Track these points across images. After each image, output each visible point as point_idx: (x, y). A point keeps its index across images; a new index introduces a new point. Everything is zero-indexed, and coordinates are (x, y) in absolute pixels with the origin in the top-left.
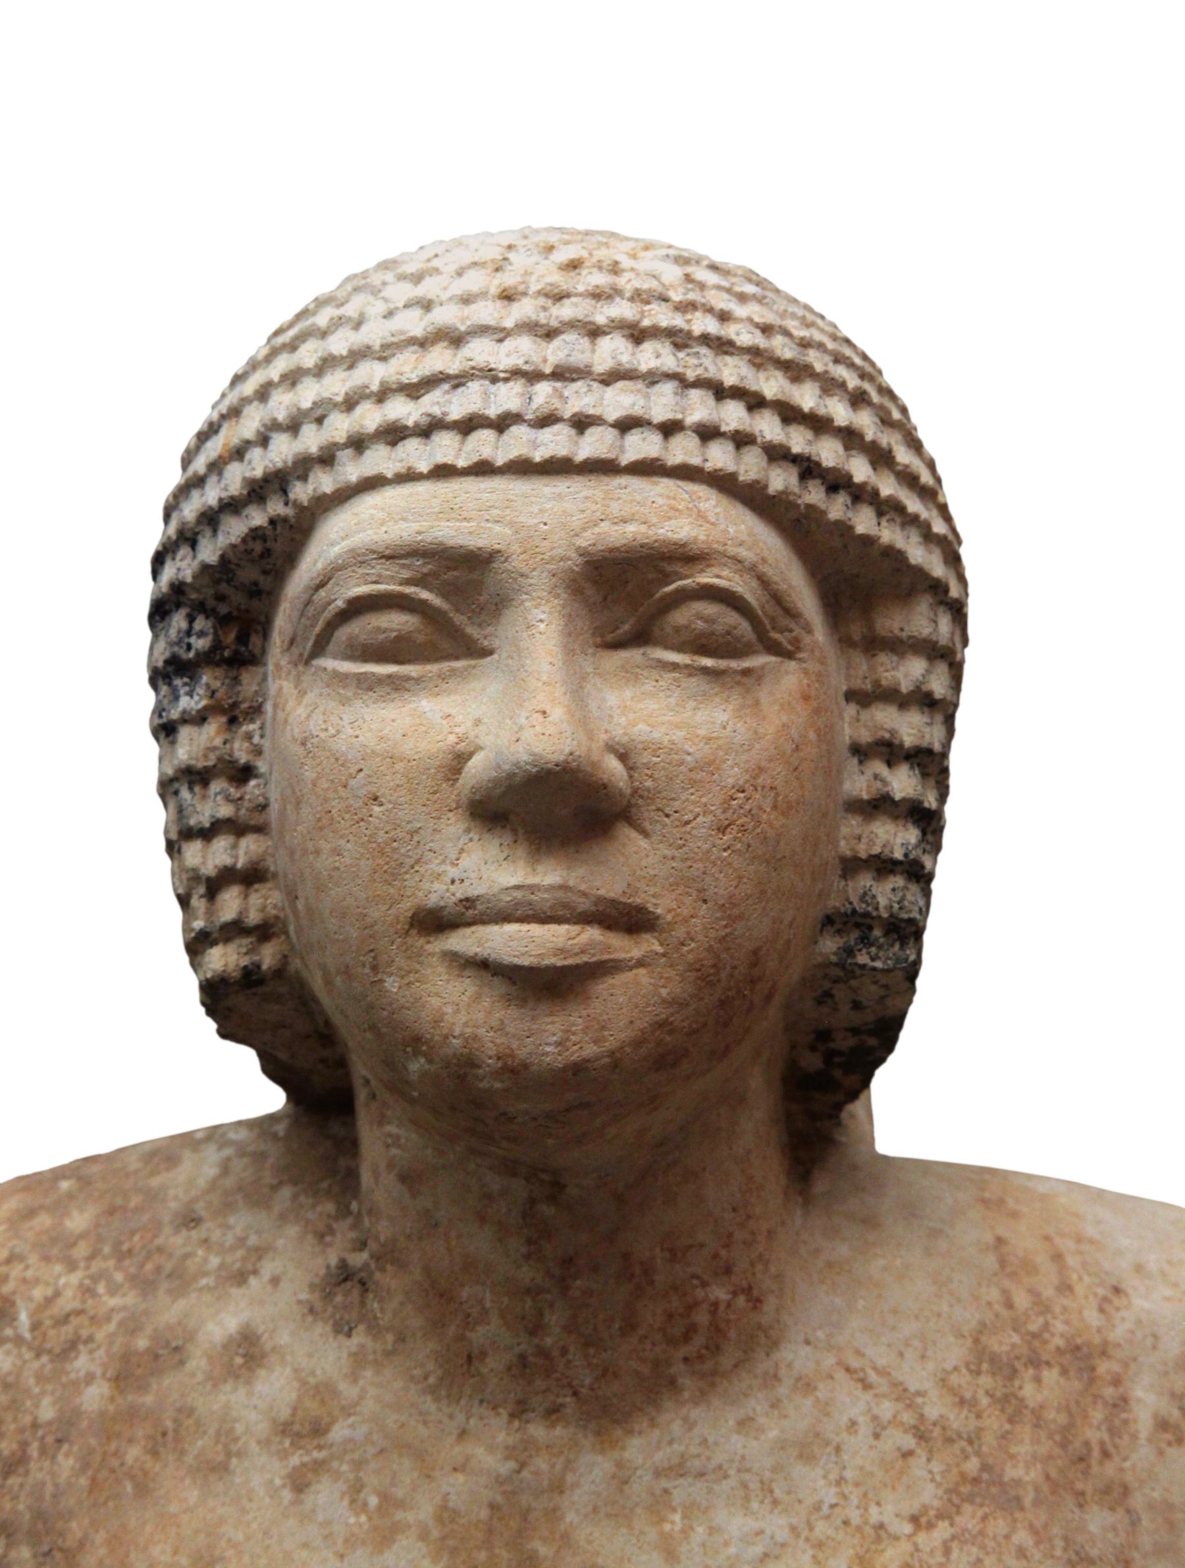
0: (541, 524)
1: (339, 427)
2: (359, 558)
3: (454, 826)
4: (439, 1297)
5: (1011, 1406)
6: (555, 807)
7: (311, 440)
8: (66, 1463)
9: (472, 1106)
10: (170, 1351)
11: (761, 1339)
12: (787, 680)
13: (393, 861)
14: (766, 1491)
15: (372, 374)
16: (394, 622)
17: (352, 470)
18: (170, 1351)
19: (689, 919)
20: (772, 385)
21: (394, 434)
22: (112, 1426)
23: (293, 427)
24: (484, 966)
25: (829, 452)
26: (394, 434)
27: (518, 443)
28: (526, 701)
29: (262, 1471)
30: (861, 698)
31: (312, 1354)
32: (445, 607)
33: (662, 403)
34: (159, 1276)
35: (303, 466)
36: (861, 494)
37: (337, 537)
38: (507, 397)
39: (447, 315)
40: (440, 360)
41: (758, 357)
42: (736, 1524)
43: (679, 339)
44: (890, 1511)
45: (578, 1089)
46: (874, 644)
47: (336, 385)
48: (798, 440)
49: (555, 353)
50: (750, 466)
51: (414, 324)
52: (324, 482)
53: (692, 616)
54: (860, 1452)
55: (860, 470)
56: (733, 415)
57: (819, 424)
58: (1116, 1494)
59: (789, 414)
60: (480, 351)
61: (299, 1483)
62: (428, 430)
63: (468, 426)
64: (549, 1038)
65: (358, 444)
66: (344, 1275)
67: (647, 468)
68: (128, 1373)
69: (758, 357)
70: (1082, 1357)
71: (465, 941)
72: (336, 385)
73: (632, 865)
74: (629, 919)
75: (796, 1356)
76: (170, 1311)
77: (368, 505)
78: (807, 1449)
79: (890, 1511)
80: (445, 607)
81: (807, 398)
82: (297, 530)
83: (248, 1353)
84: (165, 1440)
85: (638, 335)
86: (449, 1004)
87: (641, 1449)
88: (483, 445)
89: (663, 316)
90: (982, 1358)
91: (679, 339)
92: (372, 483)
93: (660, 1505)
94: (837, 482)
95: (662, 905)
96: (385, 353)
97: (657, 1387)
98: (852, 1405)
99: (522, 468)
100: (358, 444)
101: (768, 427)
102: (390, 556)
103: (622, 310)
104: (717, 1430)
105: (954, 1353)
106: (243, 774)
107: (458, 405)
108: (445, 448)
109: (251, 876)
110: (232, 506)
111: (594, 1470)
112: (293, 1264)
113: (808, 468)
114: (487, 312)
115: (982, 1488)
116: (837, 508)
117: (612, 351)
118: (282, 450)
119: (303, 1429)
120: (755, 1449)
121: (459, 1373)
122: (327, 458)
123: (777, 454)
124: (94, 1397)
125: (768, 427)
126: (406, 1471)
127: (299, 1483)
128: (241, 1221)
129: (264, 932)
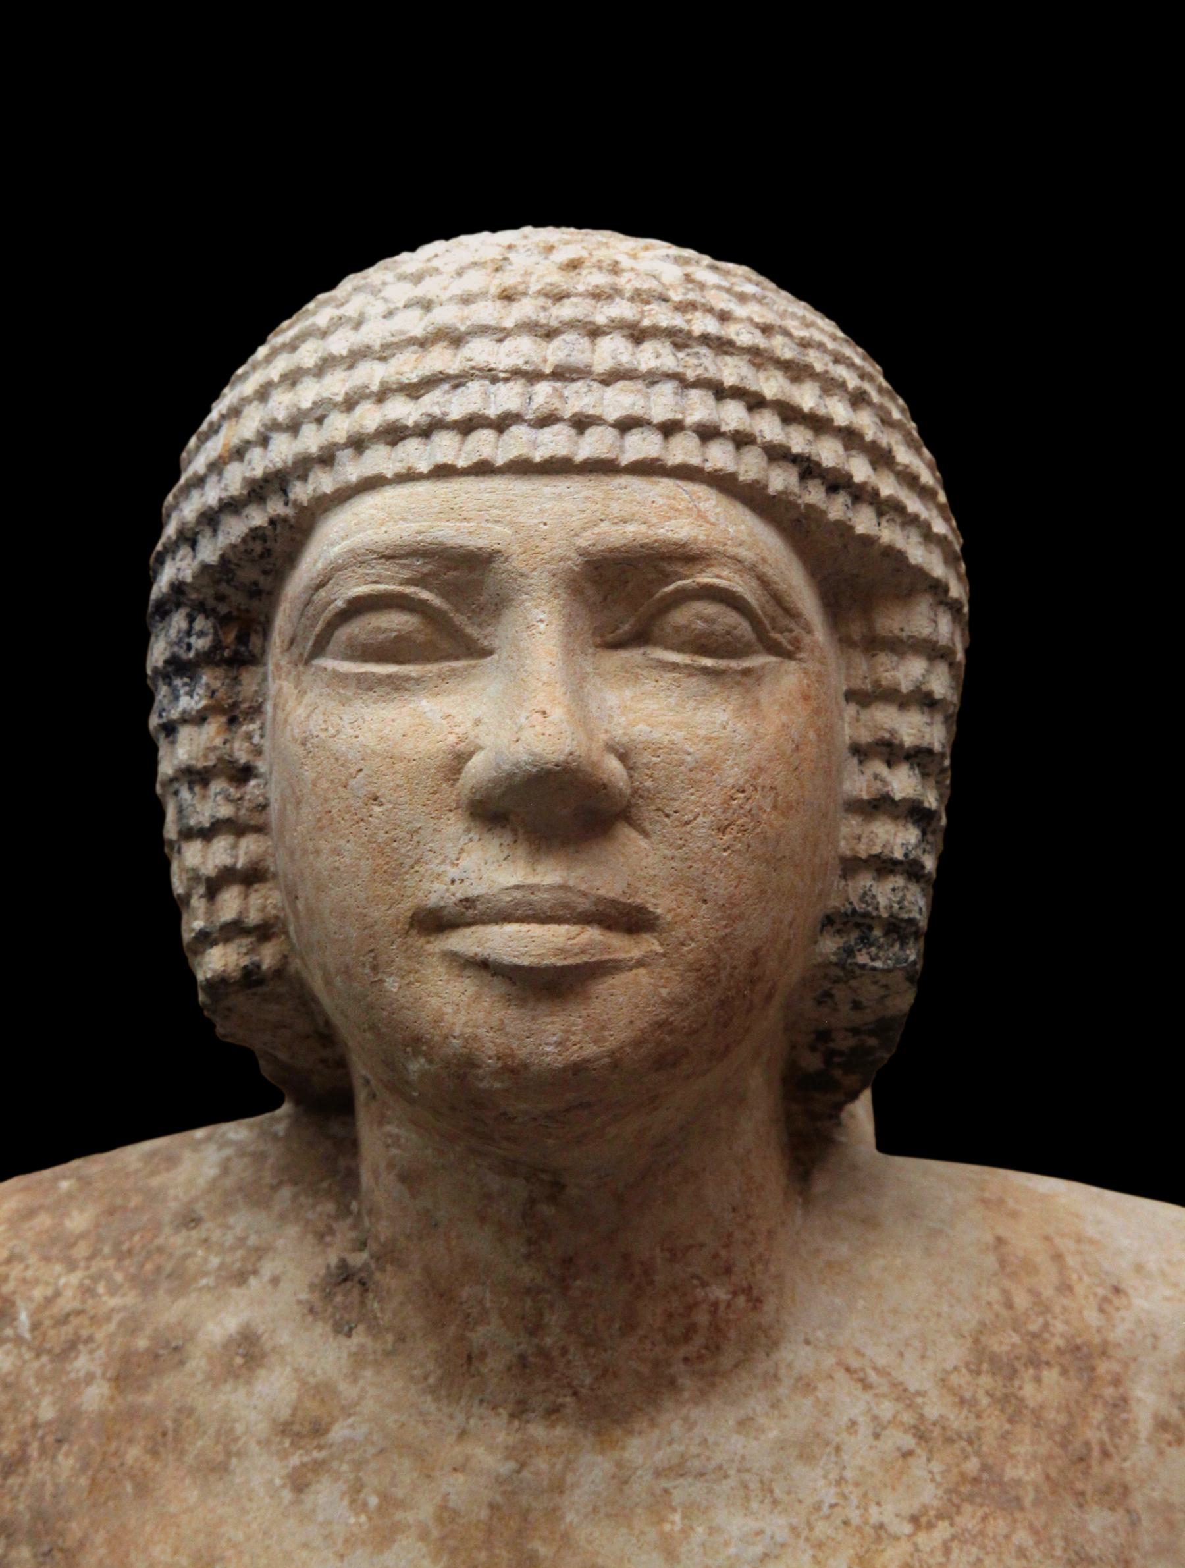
0: (541, 524)
1: (339, 427)
2: (359, 558)
3: (454, 826)
4: (439, 1297)
5: (1011, 1406)
6: (555, 807)
7: (311, 440)
8: (66, 1463)
9: (472, 1106)
10: (170, 1351)
11: (761, 1339)
12: (787, 680)
13: (393, 861)
14: (766, 1491)
15: (372, 374)
16: (394, 622)
17: (352, 470)
18: (170, 1351)
19: (689, 919)
20: (772, 385)
21: (394, 434)
22: (112, 1426)
23: (293, 427)
24: (484, 966)
25: (829, 452)
26: (394, 434)
27: (518, 443)
28: (526, 701)
29: (262, 1471)
30: (861, 698)
31: (312, 1354)
32: (445, 607)
33: (662, 403)
34: (159, 1276)
35: (303, 466)
36: (861, 494)
37: (337, 537)
38: (507, 397)
39: (447, 315)
40: (440, 360)
41: (758, 357)
42: (736, 1524)
43: (679, 339)
44: (890, 1511)
45: (578, 1089)
46: (874, 644)
47: (336, 385)
48: (798, 440)
49: (555, 353)
50: (750, 466)
51: (414, 324)
52: (324, 482)
53: (692, 616)
54: (860, 1452)
55: (860, 470)
56: (733, 415)
57: (819, 424)
58: (1116, 1494)
59: (789, 414)
60: (480, 351)
61: (299, 1483)
62: (428, 430)
63: (468, 426)
64: (549, 1038)
65: (358, 444)
66: (344, 1275)
67: (647, 468)
68: (128, 1373)
69: (758, 357)
70: (1082, 1357)
71: (465, 941)
72: (336, 385)
73: (632, 865)
74: (629, 919)
75: (796, 1356)
76: (170, 1311)
77: (368, 505)
78: (807, 1449)
79: (890, 1511)
80: (445, 607)
81: (807, 398)
82: (297, 530)
83: (248, 1353)
84: (165, 1440)
85: (638, 335)
86: (449, 1004)
87: (641, 1449)
88: (483, 445)
89: (663, 316)
90: (982, 1358)
91: (679, 339)
92: (372, 483)
93: (660, 1505)
94: (837, 482)
95: (662, 905)
96: (385, 353)
97: (657, 1387)
98: (852, 1405)
99: (522, 468)
100: (358, 444)
101: (768, 427)
102: (390, 556)
103: (622, 310)
104: (717, 1430)
105: (954, 1353)
106: (243, 774)
107: (458, 405)
108: (445, 448)
109: (251, 876)
110: (232, 506)
111: (594, 1470)
112: (293, 1264)
113: (808, 468)
114: (487, 312)
115: (982, 1488)
116: (837, 508)
117: (612, 351)
118: (282, 450)
119: (303, 1429)
120: (755, 1449)
121: (459, 1373)
122: (327, 458)
123: (777, 454)
124: (94, 1397)
125: (768, 427)
126: (406, 1471)
127: (299, 1483)
128: (241, 1221)
129: (264, 932)
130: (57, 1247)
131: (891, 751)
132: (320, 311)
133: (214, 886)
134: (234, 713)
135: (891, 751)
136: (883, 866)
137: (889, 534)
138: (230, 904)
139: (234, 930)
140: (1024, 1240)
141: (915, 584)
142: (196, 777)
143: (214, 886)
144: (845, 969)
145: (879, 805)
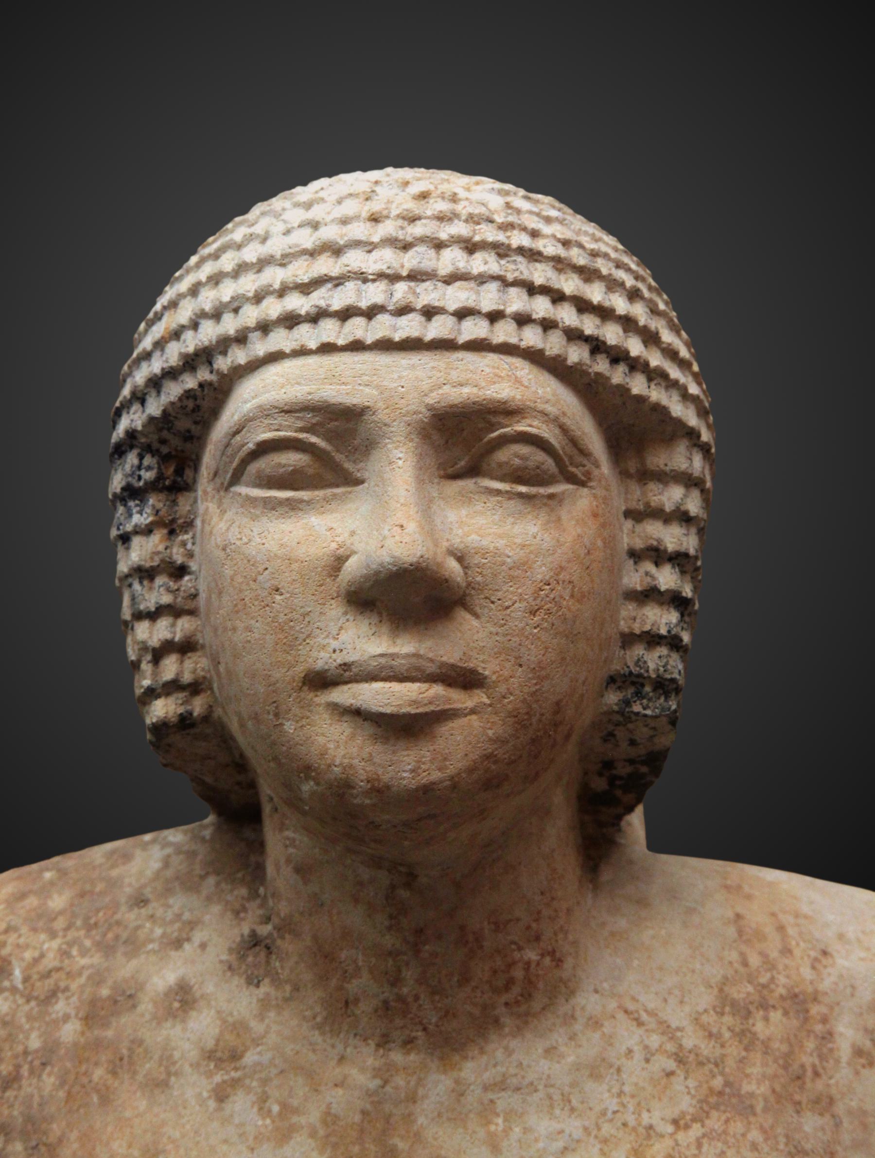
0: (399, 387)
1: (251, 315)
2: (265, 412)
3: (336, 610)
4: (324, 958)
5: (747, 1038)
6: (410, 596)
7: (230, 325)
8: (49, 1080)
9: (348, 817)
10: (126, 998)
11: (562, 989)
12: (581, 502)
13: (290, 636)
14: (565, 1101)
15: (275, 276)
16: (291, 459)
17: (260, 347)
18: (126, 998)
19: (509, 679)
20: (570, 285)
21: (291, 321)
22: (83, 1053)
23: (216, 315)
24: (357, 713)
25: (612, 334)
26: (291, 321)
27: (382, 327)
28: (389, 517)
29: (194, 1087)
30: (636, 515)
31: (230, 1000)
32: (329, 449)
33: (489, 298)
34: (118, 942)
35: (224, 344)
36: (635, 365)
37: (249, 397)
38: (374, 294)
39: (330, 233)
40: (325, 266)
41: (560, 264)
42: (543, 1125)
43: (502, 251)
44: (657, 1116)
45: (426, 804)
46: (646, 476)
47: (248, 284)
48: (589, 325)
49: (410, 261)
50: (554, 344)
51: (306, 239)
52: (239, 356)
53: (511, 455)
54: (635, 1072)
55: (635, 347)
56: (541, 307)
57: (604, 313)
58: (824, 1104)
59: (583, 306)
60: (354, 260)
61: (221, 1095)
62: (316, 317)
63: (345, 314)
64: (406, 767)
65: (264, 328)
66: (254, 942)
67: (478, 346)
68: (94, 1014)
69: (560, 264)
70: (799, 1002)
71: (343, 695)
72: (248, 284)
73: (467, 639)
74: (464, 679)
75: (588, 1001)
76: (125, 968)
77: (272, 373)
78: (596, 1070)
79: (657, 1116)
80: (329, 449)
81: (596, 294)
82: (220, 391)
83: (183, 999)
84: (122, 1064)
85: (471, 247)
86: (331, 742)
87: (473, 1070)
88: (357, 329)
89: (489, 234)
90: (725, 1003)
91: (502, 251)
92: (275, 357)
93: (487, 1111)
94: (618, 356)
95: (489, 669)
96: (284, 261)
97: (485, 1024)
98: (629, 1037)
99: (385, 345)
100: (264, 328)
101: (567, 315)
102: (288, 410)
103: (459, 229)
104: (529, 1056)
105: (705, 999)
106: (179, 571)
107: (338, 299)
108: (329, 331)
109: (185, 647)
110: (171, 374)
111: (438, 1086)
112: (216, 933)
113: (597, 346)
114: (359, 231)
115: (725, 1099)
116: (618, 375)
117: (452, 259)
118: (209, 332)
119: (224, 1055)
120: (558, 1070)
121: (339, 1014)
122: (241, 338)
123: (574, 335)
124: (70, 1032)
125: (567, 315)
126: (300, 1086)
127: (221, 1095)
128: (178, 902)
129: (195, 688)
130: (42, 921)
131: (658, 555)
132: (237, 230)
133: (158, 654)
134: (173, 527)
135: (658, 555)
136: (652, 639)
137: (656, 394)
138: (170, 668)
139: (173, 687)
140: (756, 916)
141: (675, 431)
142: (145, 574)
143: (158, 654)
144: (624, 716)
145: (649, 595)
